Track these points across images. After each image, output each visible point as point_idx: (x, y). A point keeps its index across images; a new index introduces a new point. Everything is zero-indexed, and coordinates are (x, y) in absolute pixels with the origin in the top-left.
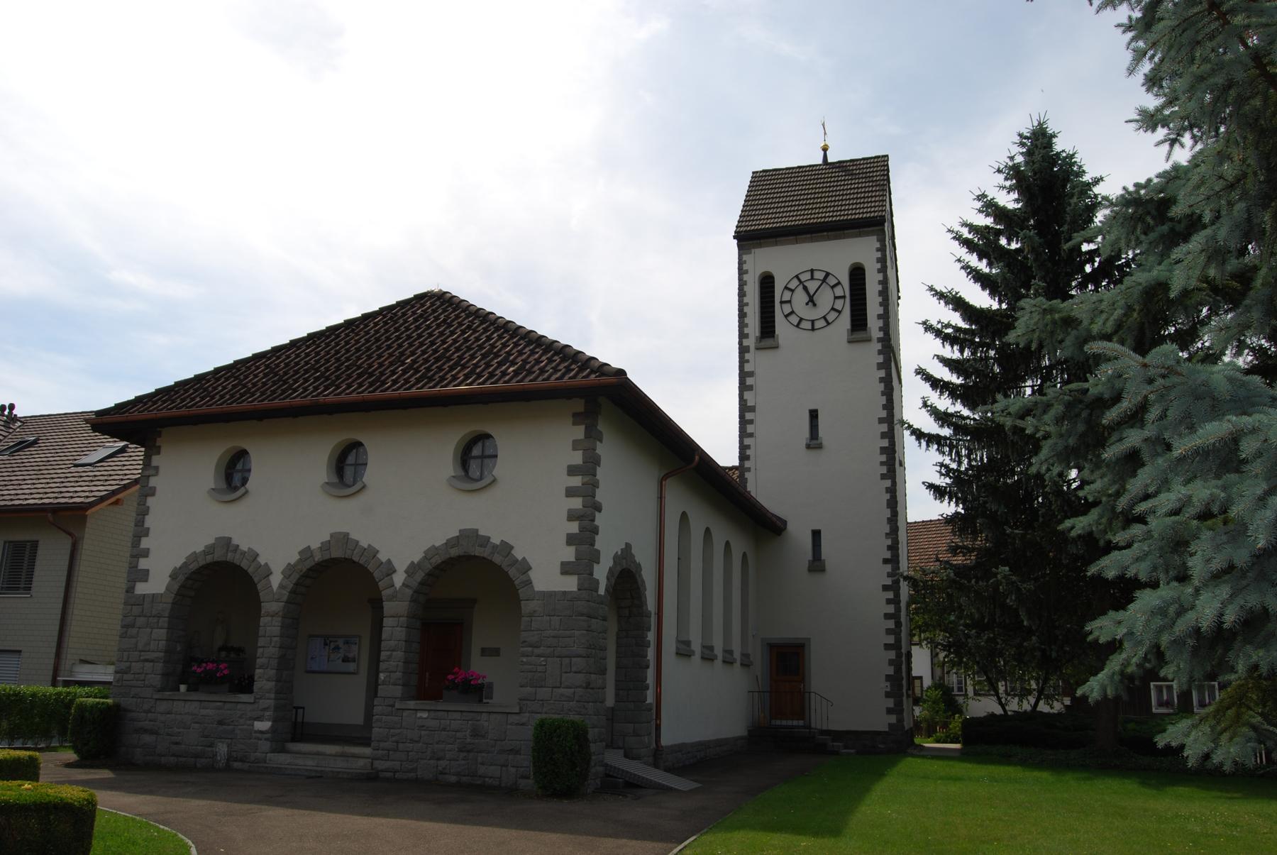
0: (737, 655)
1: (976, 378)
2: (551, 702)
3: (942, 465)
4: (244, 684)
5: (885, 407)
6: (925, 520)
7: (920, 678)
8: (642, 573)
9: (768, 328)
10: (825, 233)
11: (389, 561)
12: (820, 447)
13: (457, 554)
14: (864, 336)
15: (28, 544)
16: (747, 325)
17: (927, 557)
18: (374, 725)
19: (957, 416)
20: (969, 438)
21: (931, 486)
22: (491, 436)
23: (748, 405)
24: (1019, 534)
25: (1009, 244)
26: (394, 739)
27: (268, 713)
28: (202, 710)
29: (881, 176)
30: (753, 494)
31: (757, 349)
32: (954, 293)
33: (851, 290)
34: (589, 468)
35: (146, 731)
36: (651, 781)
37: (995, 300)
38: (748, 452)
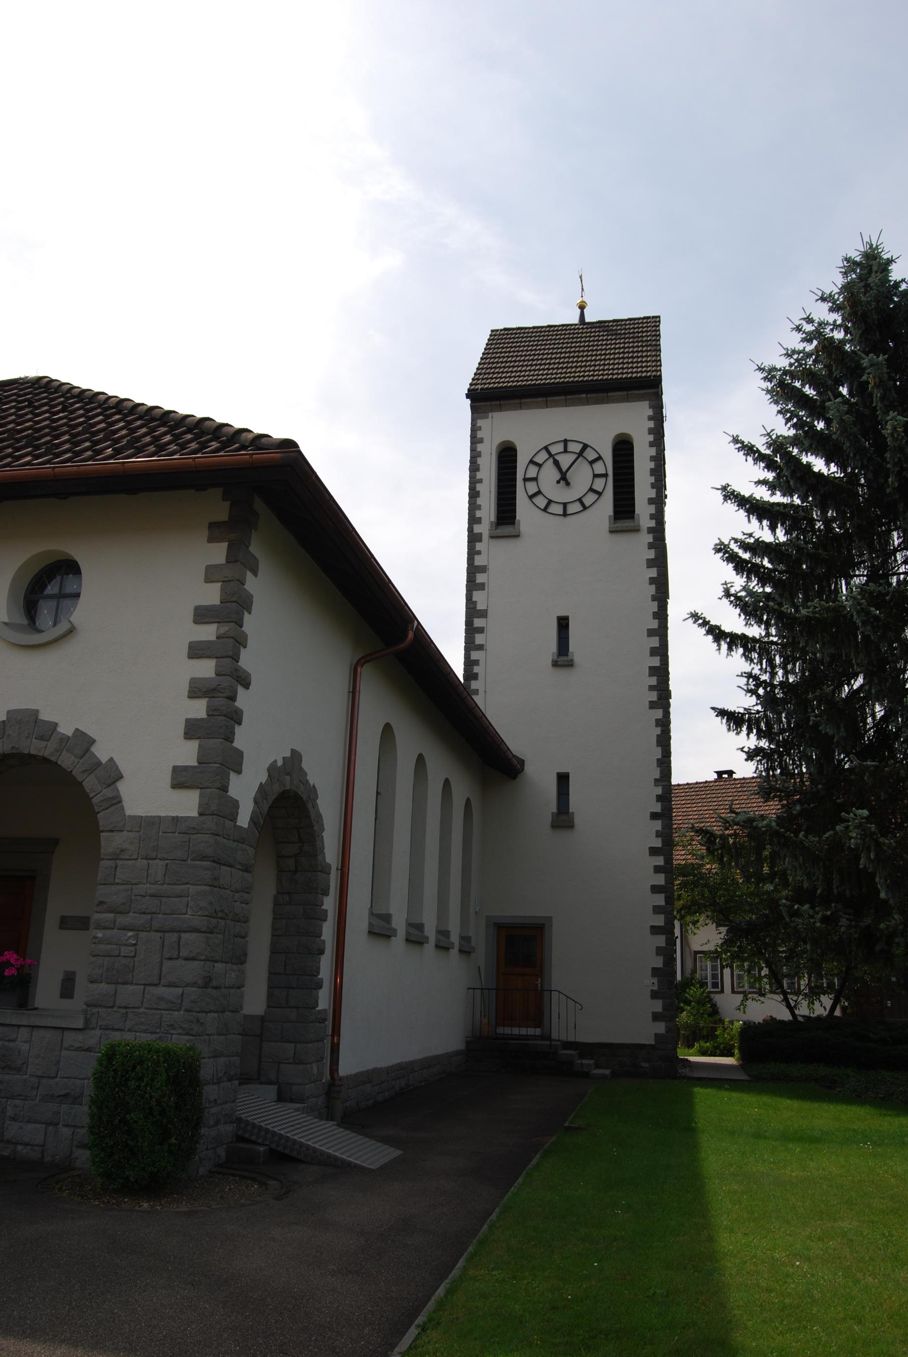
0: (455, 938)
2: (142, 1010)
3: (749, 676)
8: (319, 801)
10: (584, 395)
12: (570, 664)
14: (632, 524)
16: (479, 508)
23: (478, 608)
24: (870, 766)
29: (653, 336)
31: (492, 537)
33: (614, 468)
36: (315, 1150)
38: (476, 669)
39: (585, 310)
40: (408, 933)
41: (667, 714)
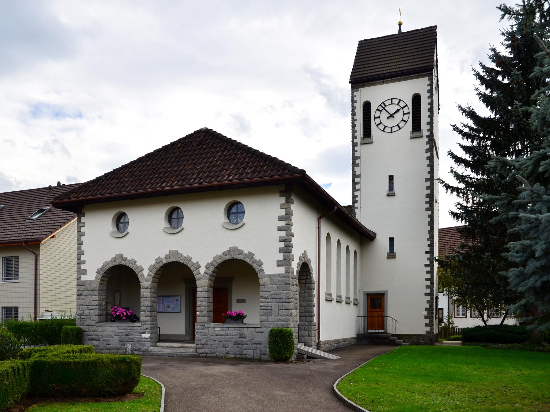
0: (352, 300)
1: (479, 157)
4: (134, 318)
5: (429, 173)
6: (448, 227)
7: (442, 309)
9: (367, 133)
10: (400, 77)
11: (197, 263)
12: (394, 195)
13: (229, 259)
14: (420, 134)
15: (13, 258)
16: (356, 131)
17: (448, 247)
18: (196, 334)
19: (468, 177)
20: (473, 189)
21: (452, 213)
22: (241, 203)
25: (503, 80)
26: (205, 340)
27: (148, 330)
28: (118, 330)
30: (359, 220)
32: (471, 109)
33: (413, 109)
34: (287, 217)
35: (94, 339)
37: (493, 113)
38: (357, 199)
39: (401, 26)
40: (337, 299)
41: (433, 213)
